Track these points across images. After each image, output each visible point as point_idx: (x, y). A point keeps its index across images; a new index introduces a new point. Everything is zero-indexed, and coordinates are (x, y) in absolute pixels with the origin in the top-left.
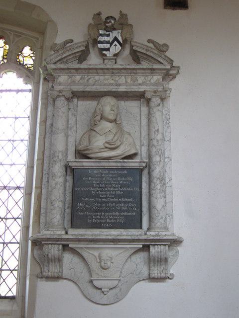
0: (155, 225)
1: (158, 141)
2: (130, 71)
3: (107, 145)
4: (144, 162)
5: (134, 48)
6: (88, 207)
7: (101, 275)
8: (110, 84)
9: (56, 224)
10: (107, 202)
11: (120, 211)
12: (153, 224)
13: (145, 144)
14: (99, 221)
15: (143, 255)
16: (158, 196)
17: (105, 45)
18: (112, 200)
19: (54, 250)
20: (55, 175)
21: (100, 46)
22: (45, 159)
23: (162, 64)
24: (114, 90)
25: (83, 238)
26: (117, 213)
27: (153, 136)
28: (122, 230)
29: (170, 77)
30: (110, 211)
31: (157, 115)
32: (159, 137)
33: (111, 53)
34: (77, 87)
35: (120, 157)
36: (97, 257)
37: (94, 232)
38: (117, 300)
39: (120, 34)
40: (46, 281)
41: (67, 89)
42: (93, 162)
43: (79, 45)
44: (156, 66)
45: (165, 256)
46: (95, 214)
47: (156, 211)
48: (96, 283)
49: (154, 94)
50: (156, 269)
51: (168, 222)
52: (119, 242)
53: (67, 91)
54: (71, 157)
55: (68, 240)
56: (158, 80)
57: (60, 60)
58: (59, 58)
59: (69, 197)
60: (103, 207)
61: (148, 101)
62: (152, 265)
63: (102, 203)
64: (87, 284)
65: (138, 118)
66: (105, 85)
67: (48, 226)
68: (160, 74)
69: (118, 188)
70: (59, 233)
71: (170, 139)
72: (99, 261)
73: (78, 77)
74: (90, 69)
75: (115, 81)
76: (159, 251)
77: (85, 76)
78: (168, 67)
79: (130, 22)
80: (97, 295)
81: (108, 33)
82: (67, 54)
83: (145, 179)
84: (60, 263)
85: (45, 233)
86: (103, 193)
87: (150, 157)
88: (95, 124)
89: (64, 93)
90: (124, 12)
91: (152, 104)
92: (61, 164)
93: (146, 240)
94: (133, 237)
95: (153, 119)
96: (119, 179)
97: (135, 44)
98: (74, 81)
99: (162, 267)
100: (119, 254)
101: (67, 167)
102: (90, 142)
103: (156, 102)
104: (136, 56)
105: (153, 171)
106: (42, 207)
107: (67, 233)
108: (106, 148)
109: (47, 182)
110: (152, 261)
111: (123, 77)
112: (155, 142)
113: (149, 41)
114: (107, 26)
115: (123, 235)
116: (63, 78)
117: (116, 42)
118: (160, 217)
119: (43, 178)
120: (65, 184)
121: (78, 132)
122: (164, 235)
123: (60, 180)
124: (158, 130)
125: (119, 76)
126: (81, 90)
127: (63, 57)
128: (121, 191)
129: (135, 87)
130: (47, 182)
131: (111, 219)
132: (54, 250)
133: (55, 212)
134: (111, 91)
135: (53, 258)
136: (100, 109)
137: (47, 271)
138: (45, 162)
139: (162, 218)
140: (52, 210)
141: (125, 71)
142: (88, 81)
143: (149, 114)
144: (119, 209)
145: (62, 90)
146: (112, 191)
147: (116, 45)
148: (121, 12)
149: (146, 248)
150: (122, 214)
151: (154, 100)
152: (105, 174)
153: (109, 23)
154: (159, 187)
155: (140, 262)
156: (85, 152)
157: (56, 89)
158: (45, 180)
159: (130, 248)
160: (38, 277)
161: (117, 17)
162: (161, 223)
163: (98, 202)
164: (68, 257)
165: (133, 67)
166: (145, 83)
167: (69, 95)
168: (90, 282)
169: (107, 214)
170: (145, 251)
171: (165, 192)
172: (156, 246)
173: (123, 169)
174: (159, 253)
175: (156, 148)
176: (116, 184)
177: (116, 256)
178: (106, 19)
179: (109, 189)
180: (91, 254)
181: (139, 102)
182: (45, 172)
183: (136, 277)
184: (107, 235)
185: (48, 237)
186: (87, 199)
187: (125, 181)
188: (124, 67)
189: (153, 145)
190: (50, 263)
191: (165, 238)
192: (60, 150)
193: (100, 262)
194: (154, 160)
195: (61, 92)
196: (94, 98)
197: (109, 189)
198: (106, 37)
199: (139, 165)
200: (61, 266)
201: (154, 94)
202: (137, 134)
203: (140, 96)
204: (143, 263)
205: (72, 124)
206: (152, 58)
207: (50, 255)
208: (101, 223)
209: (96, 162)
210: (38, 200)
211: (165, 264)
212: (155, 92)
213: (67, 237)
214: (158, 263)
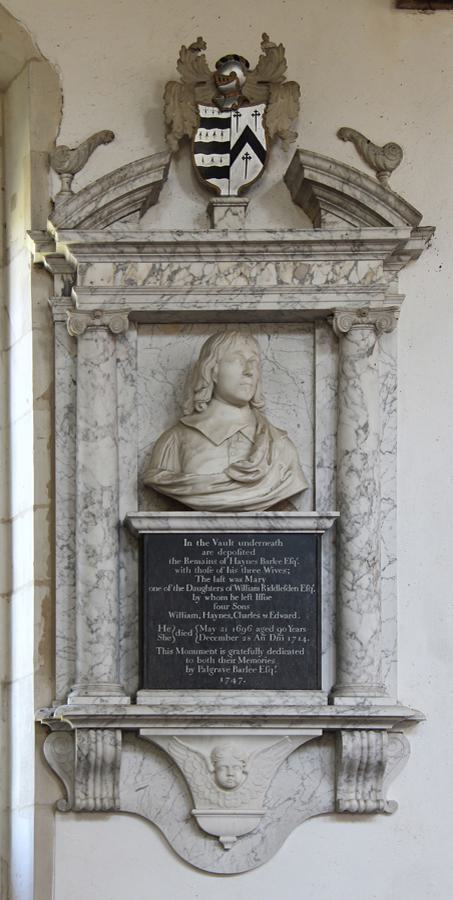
0: (354, 680)
1: (365, 456)
2: (292, 248)
3: (237, 475)
4: (329, 518)
5: (307, 174)
6: (184, 634)
7: (218, 805)
8: (235, 289)
9: (105, 678)
10: (233, 623)
11: (266, 645)
12: (348, 679)
13: (326, 464)
14: (212, 671)
15: (321, 754)
16: (364, 607)
17: (216, 157)
18: (245, 616)
19: (104, 744)
20: (94, 551)
21: (202, 160)
22: (58, 506)
23: (389, 224)
24: (244, 307)
25: (178, 713)
26: (258, 651)
27: (350, 442)
28: (272, 694)
29: (403, 258)
30: (240, 645)
31: (366, 382)
32: (369, 445)
33: (232, 185)
34: (143, 299)
35: (260, 506)
36: (209, 761)
37: (203, 699)
38: (256, 862)
39: (260, 119)
40: (78, 819)
41: (114, 307)
42: (198, 518)
43: (148, 165)
44: (369, 234)
45: (378, 758)
46: (201, 652)
47: (357, 646)
48: (204, 823)
49: (359, 320)
50: (353, 788)
51: (384, 671)
52: (266, 722)
53: (115, 312)
54: (128, 506)
55: (138, 718)
56: (372, 272)
57: (91, 215)
58: (90, 208)
59: (128, 608)
60: (223, 634)
61: (339, 339)
62: (343, 778)
63: (220, 623)
64: (182, 824)
65: (307, 387)
66: (219, 292)
67: (90, 685)
68: (376, 255)
69: (259, 585)
70: (115, 701)
71: (395, 447)
72: (212, 768)
73: (143, 268)
74: (178, 244)
75: (248, 279)
76: (365, 744)
77: (164, 265)
78: (404, 233)
79: (290, 75)
80: (203, 852)
81: (224, 115)
82: (112, 196)
83: (326, 558)
84: (114, 774)
85: (79, 703)
86: (221, 598)
87: (340, 500)
88: (196, 411)
89: (106, 319)
90: (274, 40)
91: (351, 349)
92: (108, 524)
93: (333, 719)
94: (302, 712)
95: (354, 394)
96: (262, 561)
97: (311, 161)
98: (131, 282)
99: (369, 785)
100: (264, 751)
101: (125, 528)
102: (183, 460)
103: (363, 344)
104: (307, 195)
105: (349, 539)
106: (58, 633)
107: (134, 701)
108: (233, 481)
109: (68, 568)
110: (339, 768)
111: (271, 267)
112: (356, 461)
113: (343, 134)
114: (221, 93)
115: (278, 706)
116: (100, 272)
117: (247, 148)
118: (367, 660)
119: (58, 559)
120: (118, 572)
121: (145, 430)
122: (382, 706)
123: (109, 565)
124: (366, 425)
125: (258, 262)
126: (154, 308)
127: (101, 205)
128: (268, 594)
129: (303, 298)
130: (68, 568)
131: (243, 666)
132: (104, 745)
133: (100, 648)
134: (237, 311)
135: (99, 762)
136: (212, 370)
137: (82, 796)
138: (58, 514)
139: (372, 662)
140: (91, 643)
141: (279, 249)
142: (171, 279)
143: (340, 377)
144: (263, 638)
145: (101, 311)
146: (245, 594)
147: (247, 158)
148: (265, 36)
149: (331, 738)
150: (271, 652)
151: (356, 335)
152: (226, 548)
153: (228, 79)
154: (365, 582)
155: (312, 772)
156: (174, 491)
157: (83, 308)
158: (61, 564)
159: (291, 737)
160: (55, 809)
161: (254, 57)
162: (370, 675)
163: (209, 622)
164: (132, 761)
165: (304, 236)
166: (327, 284)
167: (120, 323)
168: (187, 821)
169: (232, 652)
170: (325, 745)
171: (378, 593)
172: (357, 734)
173: (271, 536)
174: (366, 750)
175: (360, 477)
176: (255, 575)
177: (256, 757)
178: (218, 66)
179: (237, 588)
180: (191, 754)
181: (309, 337)
182: (60, 543)
183: (301, 808)
184: (238, 707)
185: (92, 712)
186: (182, 615)
187: (276, 567)
188: (277, 237)
189: (351, 470)
190: (91, 776)
191: (382, 714)
192: (106, 483)
193: (215, 772)
194: (353, 510)
195: (98, 317)
196: (182, 326)
197: (237, 588)
198: (218, 131)
199: (316, 526)
200: (116, 783)
201: (359, 320)
202: (304, 434)
203: (317, 323)
204: (319, 774)
205: (127, 408)
206: (358, 203)
207: (93, 755)
208: (218, 675)
209: (203, 518)
210: (43, 614)
211: (377, 777)
212: (361, 313)
213: (133, 711)
214: (359, 775)
